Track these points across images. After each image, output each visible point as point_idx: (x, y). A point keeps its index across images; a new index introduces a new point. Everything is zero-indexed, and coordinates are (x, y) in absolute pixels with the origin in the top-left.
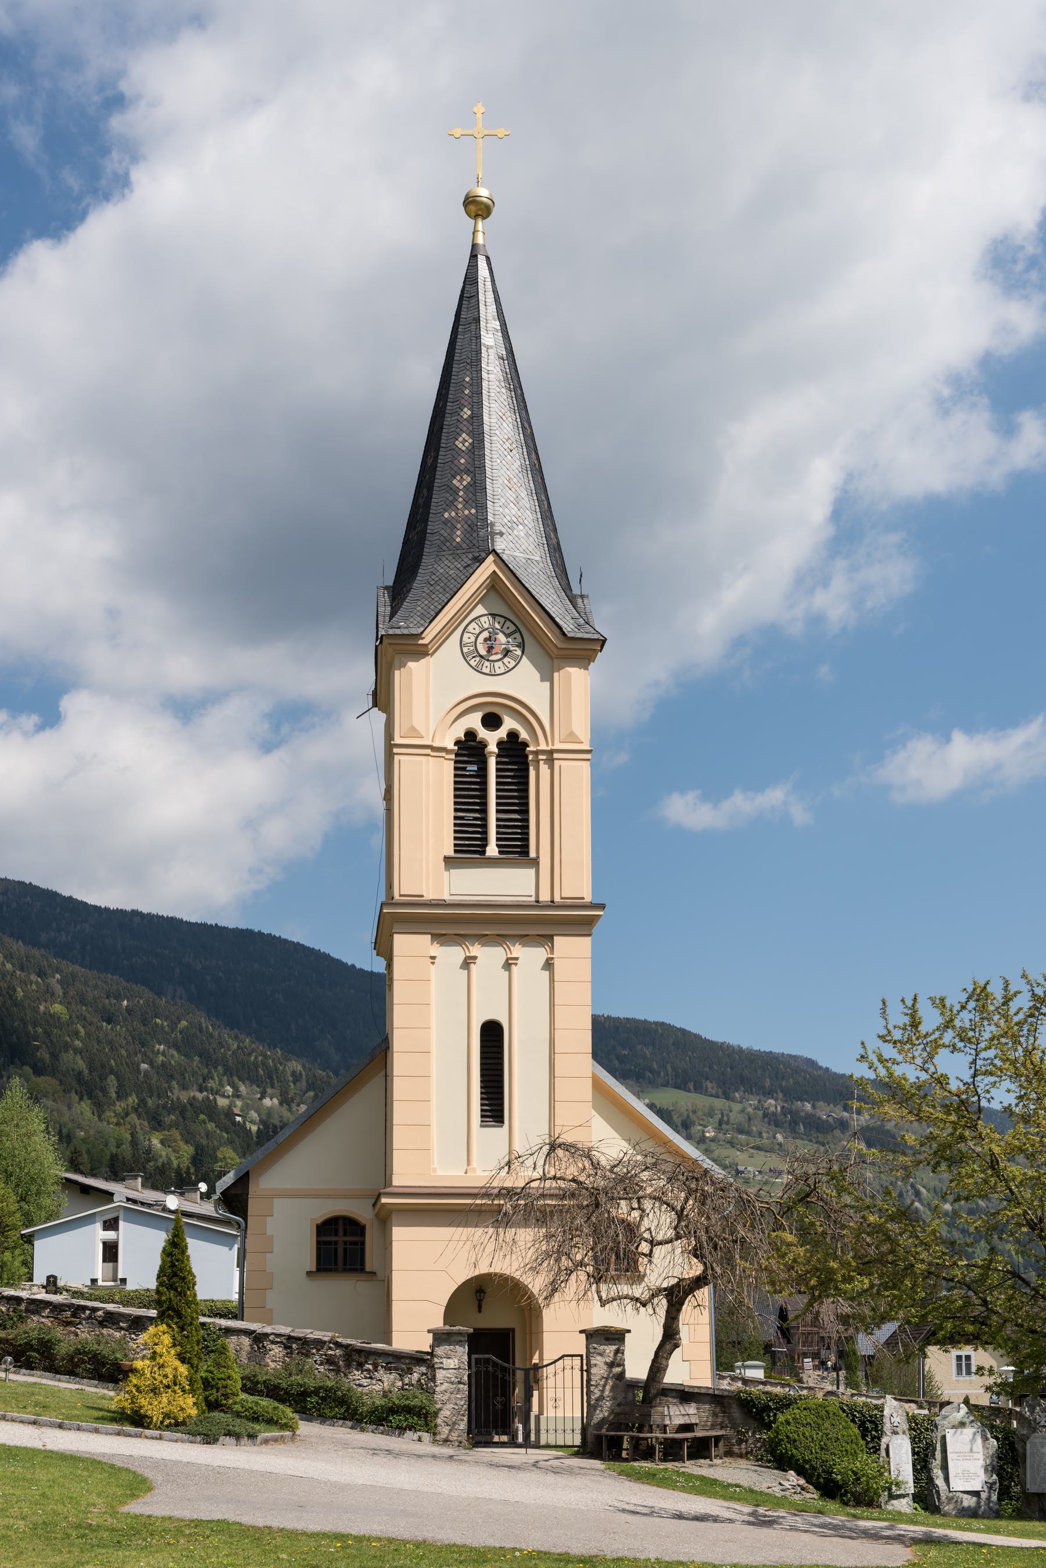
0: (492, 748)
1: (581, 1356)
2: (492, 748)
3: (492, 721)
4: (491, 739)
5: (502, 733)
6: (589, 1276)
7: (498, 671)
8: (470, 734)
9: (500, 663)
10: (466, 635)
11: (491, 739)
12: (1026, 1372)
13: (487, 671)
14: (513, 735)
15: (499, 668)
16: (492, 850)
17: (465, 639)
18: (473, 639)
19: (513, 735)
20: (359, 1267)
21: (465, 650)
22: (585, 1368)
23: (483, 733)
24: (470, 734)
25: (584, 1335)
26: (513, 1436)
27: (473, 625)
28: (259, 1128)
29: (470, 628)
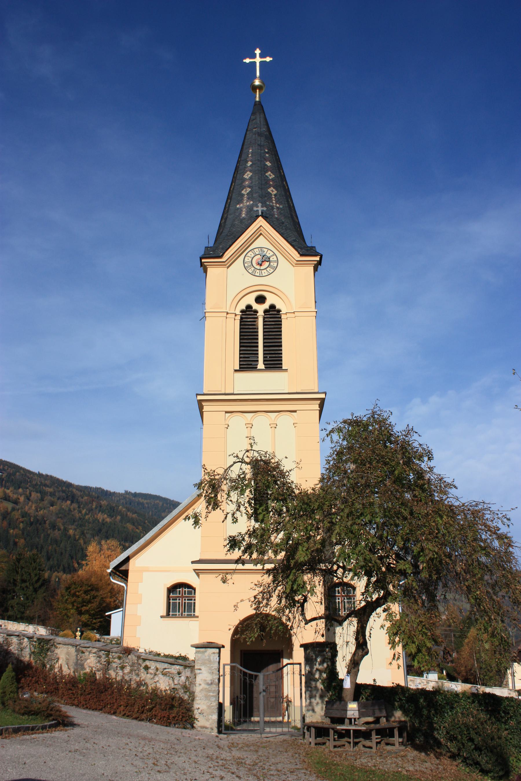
0: (261, 313)
1: (300, 664)
2: (261, 313)
3: (260, 300)
4: (260, 308)
5: (266, 306)
6: (302, 606)
7: (264, 275)
8: (249, 307)
9: (265, 271)
10: (246, 258)
11: (260, 308)
12: (442, 739)
13: (258, 275)
14: (272, 307)
15: (264, 273)
16: (261, 365)
17: (246, 260)
18: (250, 260)
19: (272, 307)
20: (171, 613)
21: (246, 265)
22: (221, 678)
23: (255, 306)
24: (249, 307)
25: (303, 649)
26: (232, 729)
27: (250, 253)
28: (275, 566)
29: (249, 255)
